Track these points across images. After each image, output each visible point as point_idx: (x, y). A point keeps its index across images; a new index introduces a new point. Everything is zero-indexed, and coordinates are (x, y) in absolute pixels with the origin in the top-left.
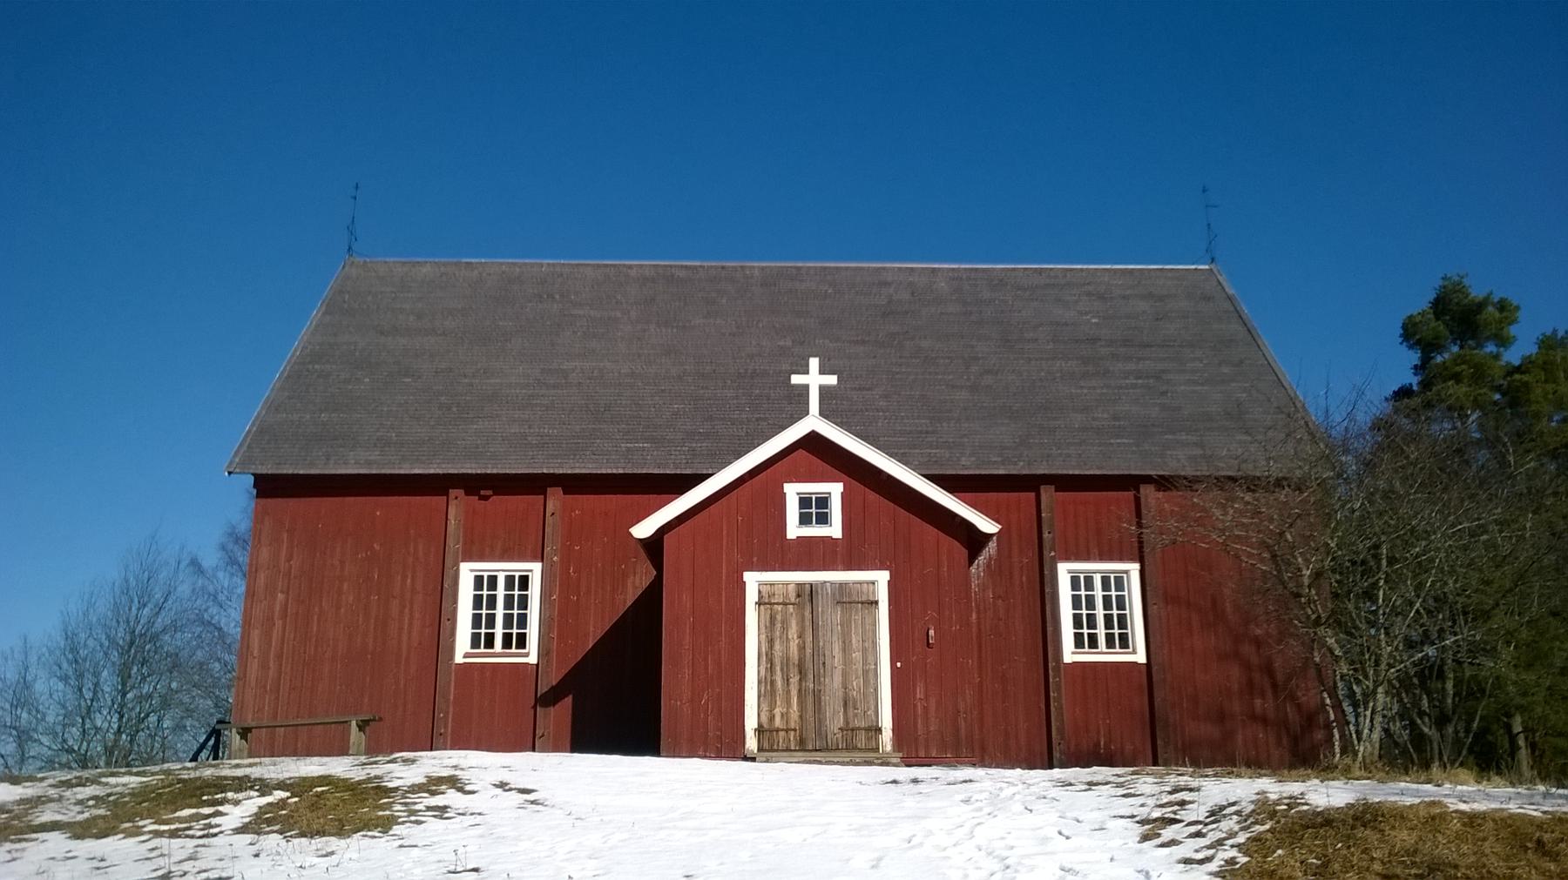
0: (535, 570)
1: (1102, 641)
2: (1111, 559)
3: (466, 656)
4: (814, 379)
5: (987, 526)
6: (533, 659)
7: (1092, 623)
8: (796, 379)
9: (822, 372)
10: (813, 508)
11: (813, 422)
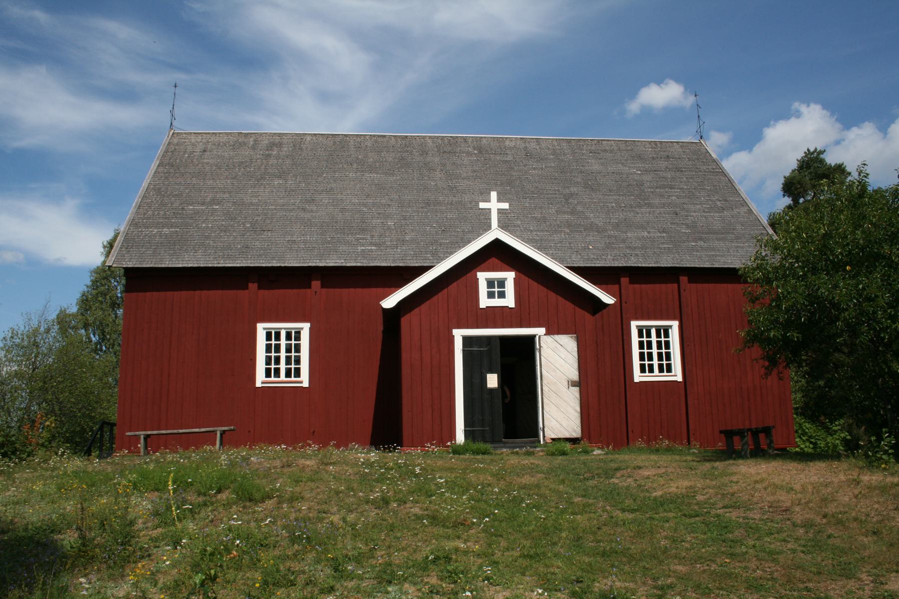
0: (305, 327)
1: (283, 373)
3: (263, 383)
4: (494, 205)
6: (306, 384)
7: (650, 357)
9: (499, 200)
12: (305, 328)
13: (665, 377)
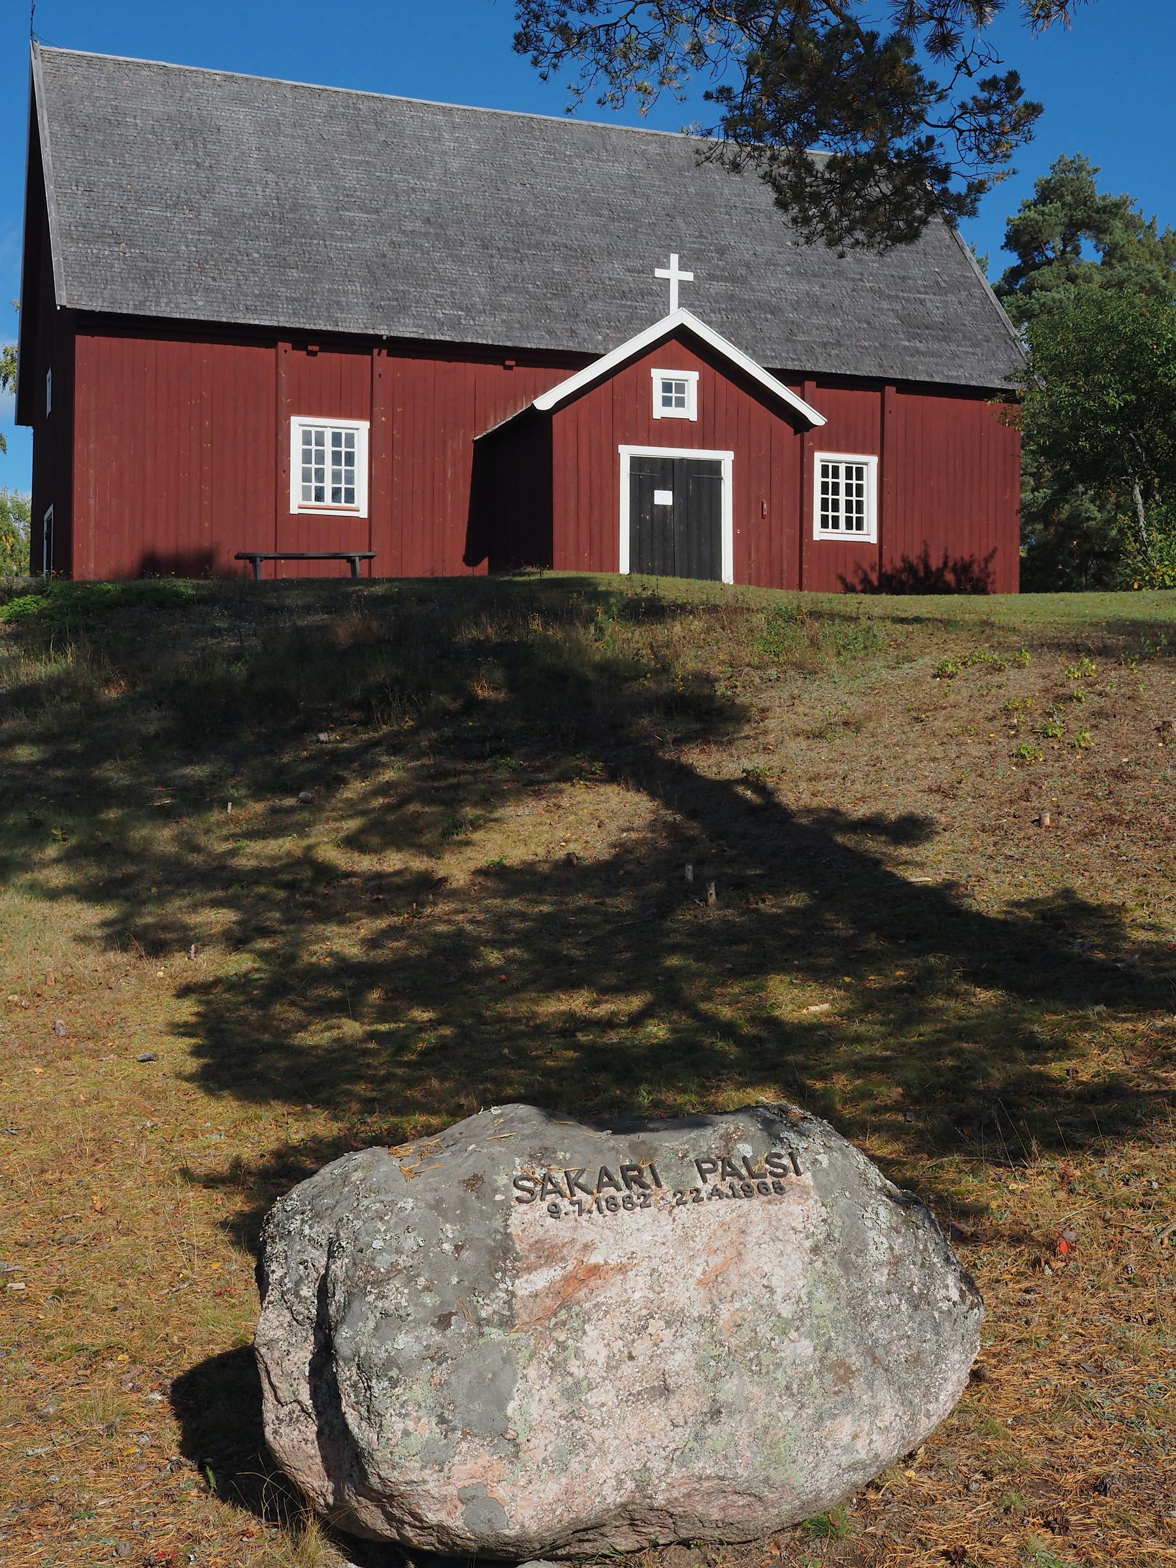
0: (361, 429)
2: (855, 451)
4: (674, 273)
5: (816, 418)
6: (363, 514)
8: (659, 273)
10: (677, 394)
11: (678, 316)
12: (361, 429)
13: (853, 536)
